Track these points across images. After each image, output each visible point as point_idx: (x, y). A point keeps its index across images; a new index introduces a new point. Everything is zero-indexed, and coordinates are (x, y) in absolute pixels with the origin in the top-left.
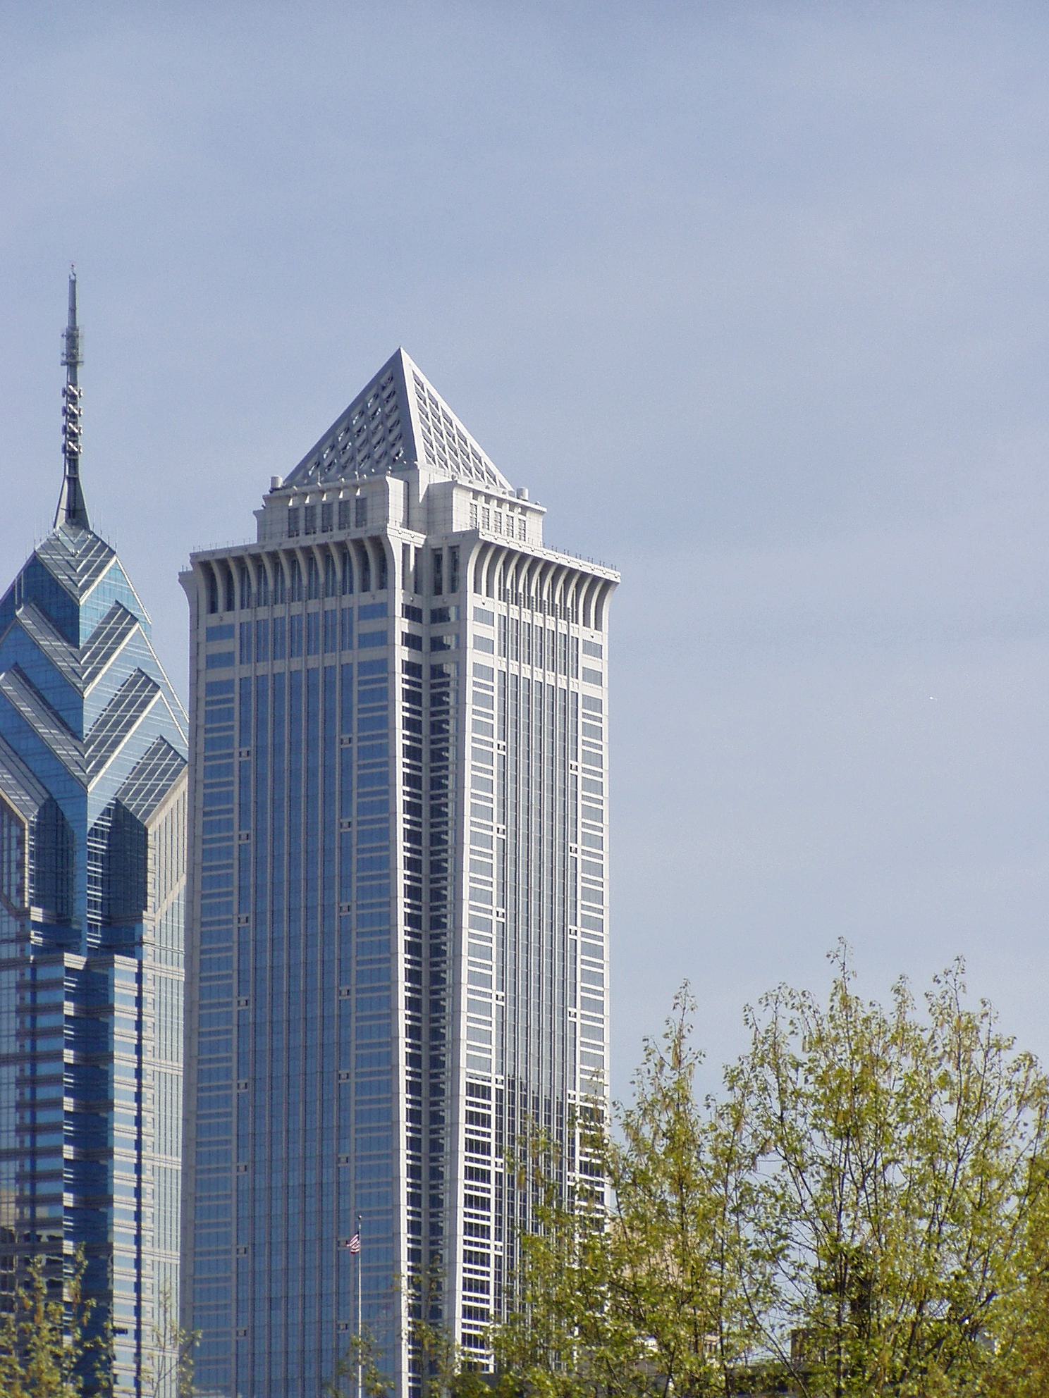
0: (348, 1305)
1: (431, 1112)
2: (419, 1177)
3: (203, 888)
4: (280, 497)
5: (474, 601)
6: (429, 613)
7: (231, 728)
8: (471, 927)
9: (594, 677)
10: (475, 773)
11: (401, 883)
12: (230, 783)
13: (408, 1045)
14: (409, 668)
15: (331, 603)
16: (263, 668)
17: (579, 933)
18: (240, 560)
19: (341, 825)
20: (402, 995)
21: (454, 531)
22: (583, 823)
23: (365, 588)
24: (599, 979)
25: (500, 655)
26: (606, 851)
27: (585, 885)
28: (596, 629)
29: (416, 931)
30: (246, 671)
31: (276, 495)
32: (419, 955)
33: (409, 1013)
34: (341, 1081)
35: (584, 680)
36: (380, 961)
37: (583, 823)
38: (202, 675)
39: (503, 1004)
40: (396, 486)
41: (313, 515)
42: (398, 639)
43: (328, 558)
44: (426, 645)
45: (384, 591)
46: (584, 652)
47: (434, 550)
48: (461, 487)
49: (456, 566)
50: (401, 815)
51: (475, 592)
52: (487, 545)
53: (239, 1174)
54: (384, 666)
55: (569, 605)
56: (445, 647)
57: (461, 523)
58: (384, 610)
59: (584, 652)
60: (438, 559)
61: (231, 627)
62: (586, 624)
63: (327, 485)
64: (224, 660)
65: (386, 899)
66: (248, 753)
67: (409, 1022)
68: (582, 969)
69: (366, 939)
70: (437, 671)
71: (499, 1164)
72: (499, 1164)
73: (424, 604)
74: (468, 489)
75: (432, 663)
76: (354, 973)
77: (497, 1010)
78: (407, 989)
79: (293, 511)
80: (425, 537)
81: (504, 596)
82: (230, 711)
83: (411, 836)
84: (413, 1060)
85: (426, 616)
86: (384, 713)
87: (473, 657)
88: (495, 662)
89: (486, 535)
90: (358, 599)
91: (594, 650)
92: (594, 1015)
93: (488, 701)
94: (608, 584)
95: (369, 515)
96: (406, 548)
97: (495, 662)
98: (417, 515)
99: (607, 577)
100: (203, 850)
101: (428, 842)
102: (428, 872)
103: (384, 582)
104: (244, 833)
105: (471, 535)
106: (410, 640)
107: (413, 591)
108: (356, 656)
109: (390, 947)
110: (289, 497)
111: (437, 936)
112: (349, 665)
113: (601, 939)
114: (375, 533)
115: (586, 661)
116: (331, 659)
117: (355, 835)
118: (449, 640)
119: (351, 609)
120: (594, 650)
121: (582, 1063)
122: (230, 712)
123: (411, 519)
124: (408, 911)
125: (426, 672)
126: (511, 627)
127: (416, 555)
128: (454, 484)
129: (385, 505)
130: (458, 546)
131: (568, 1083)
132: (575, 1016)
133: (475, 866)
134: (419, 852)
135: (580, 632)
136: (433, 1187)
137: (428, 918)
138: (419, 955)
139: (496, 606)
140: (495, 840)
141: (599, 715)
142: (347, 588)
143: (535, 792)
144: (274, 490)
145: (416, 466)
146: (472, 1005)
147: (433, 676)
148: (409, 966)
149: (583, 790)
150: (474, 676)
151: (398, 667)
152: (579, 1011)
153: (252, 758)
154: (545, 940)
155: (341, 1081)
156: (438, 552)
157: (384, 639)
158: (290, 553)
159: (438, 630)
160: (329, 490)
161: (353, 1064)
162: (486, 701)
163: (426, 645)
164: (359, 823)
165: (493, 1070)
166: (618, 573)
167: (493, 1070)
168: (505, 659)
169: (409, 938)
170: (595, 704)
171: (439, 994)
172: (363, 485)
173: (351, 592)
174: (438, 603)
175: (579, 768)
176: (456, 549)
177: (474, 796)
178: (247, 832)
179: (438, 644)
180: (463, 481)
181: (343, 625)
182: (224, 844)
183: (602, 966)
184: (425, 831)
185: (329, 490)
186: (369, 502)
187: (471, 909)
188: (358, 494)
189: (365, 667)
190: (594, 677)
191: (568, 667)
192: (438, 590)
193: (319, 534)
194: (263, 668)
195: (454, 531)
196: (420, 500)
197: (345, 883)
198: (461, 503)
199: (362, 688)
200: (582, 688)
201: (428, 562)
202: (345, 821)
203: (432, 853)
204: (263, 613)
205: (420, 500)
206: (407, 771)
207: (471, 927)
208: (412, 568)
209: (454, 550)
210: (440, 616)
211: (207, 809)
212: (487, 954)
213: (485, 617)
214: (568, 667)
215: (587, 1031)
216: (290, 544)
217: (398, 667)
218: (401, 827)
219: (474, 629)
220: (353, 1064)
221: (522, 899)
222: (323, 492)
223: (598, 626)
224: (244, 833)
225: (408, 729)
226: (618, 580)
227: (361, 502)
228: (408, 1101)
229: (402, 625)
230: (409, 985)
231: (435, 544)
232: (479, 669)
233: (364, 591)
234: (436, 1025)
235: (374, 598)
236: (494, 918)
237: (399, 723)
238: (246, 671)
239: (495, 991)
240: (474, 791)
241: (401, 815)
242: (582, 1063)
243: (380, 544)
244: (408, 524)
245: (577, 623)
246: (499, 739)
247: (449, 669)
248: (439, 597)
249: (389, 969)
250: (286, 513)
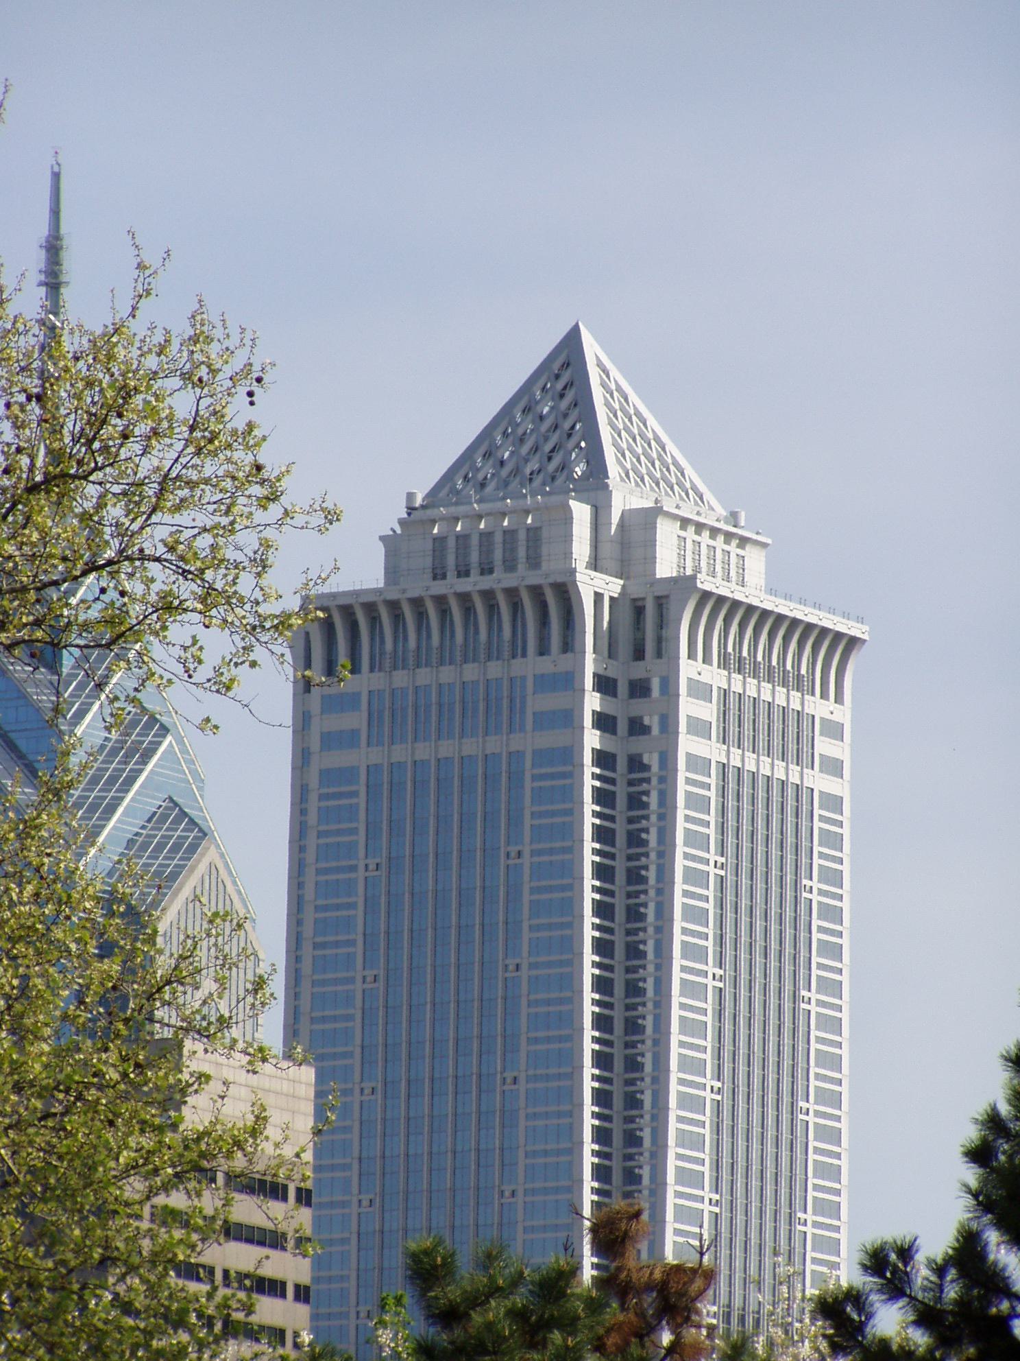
0: (516, 1164)
1: (625, 1131)
2: (610, 1030)
3: (314, 972)
4: (422, 522)
5: (688, 669)
6: (627, 684)
7: (352, 943)
8: (677, 1183)
9: (833, 767)
10: (686, 900)
11: (589, 934)
12: (355, 794)
13: (595, 1154)
14: (602, 758)
15: (495, 669)
16: (400, 753)
17: (811, 1112)
18: (370, 608)
19: (508, 855)
20: (589, 1161)
21: (658, 576)
22: (819, 927)
23: (543, 651)
24: (835, 1173)
25: (718, 742)
26: (845, 1002)
27: (823, 862)
28: (836, 702)
29: (607, 999)
30: (376, 756)
31: (416, 517)
32: (611, 1032)
33: (597, 1072)
34: (506, 1088)
35: (821, 771)
36: (559, 1076)
37: (819, 927)
38: (315, 759)
39: (719, 1098)
40: (581, 512)
41: (467, 547)
42: (588, 720)
43: (492, 608)
44: (622, 727)
45: (569, 655)
46: (821, 734)
47: (634, 600)
48: (669, 515)
49: (665, 621)
50: (589, 881)
51: (689, 658)
52: (706, 595)
53: (363, 1098)
54: (570, 754)
55: (803, 671)
56: (645, 730)
57: (665, 568)
58: (570, 682)
59: (821, 734)
60: (639, 611)
61: (355, 697)
62: (824, 695)
63: (487, 507)
64: (348, 739)
65: (569, 919)
66: (373, 1091)
67: (597, 972)
68: (815, 1198)
69: (541, 1047)
70: (636, 763)
71: (715, 1089)
72: (715, 1089)
73: (621, 673)
74: (675, 517)
75: (632, 678)
76: (523, 1054)
77: (714, 991)
78: (595, 1003)
79: (440, 541)
80: (621, 582)
81: (724, 663)
82: (353, 809)
83: (601, 872)
84: (601, 1097)
85: (622, 689)
86: (568, 932)
87: (687, 744)
88: (712, 750)
89: (706, 583)
90: (531, 666)
91: (834, 730)
92: (828, 1221)
93: (703, 805)
94: (853, 642)
95: (545, 550)
96: (598, 597)
97: (712, 750)
98: (607, 550)
99: (853, 633)
100: (319, 808)
101: (624, 878)
102: (624, 882)
103: (570, 644)
104: (370, 973)
105: (685, 583)
106: (604, 722)
107: (606, 653)
108: (529, 741)
109: (571, 982)
110: (434, 522)
111: (635, 932)
112: (520, 755)
113: (840, 1009)
114: (560, 579)
115: (824, 746)
116: (494, 744)
117: (527, 871)
118: (652, 721)
119: (524, 678)
120: (834, 730)
121: (813, 1250)
122: (352, 810)
123: (600, 555)
124: (597, 897)
125: (622, 764)
126: (732, 701)
127: (610, 607)
128: (657, 511)
129: (568, 538)
130: (667, 597)
131: (798, 1203)
132: (805, 1224)
133: (689, 913)
134: (612, 781)
135: (818, 707)
136: (630, 1082)
137: (624, 832)
138: (611, 1032)
139: (715, 676)
140: (712, 879)
141: (838, 817)
142: (517, 650)
143: (759, 924)
144: (411, 509)
145: (607, 486)
146: (681, 1212)
147: (631, 769)
148: (597, 1009)
149: (819, 918)
150: (687, 770)
151: (588, 758)
152: (810, 1217)
153: (383, 872)
154: (770, 1121)
155: (506, 1088)
156: (640, 603)
157: (570, 719)
158: (440, 600)
159: (637, 707)
160: (488, 514)
161: (527, 838)
162: (701, 804)
163: (622, 727)
164: (532, 966)
165: (709, 1075)
166: (865, 628)
167: (709, 1075)
168: (725, 747)
169: (597, 859)
170: (834, 803)
171: (636, 1009)
172: (537, 509)
173: (524, 655)
174: (638, 671)
175: (812, 999)
176: (664, 601)
177: (683, 1006)
178: (375, 972)
179: (637, 727)
180: (668, 506)
181: (511, 700)
182: (345, 913)
183: (838, 1156)
184: (620, 865)
185: (488, 514)
186: (545, 533)
187: (682, 971)
188: (529, 521)
189: (541, 756)
190: (833, 767)
191: (802, 755)
192: (639, 654)
193: (474, 576)
194: (400, 753)
195: (658, 576)
196: (613, 533)
197: (514, 821)
198: (666, 534)
199: (537, 784)
200: (818, 781)
201: (626, 617)
202: (511, 962)
203: (629, 895)
204: (401, 678)
205: (613, 533)
206: (597, 784)
207: (677, 1183)
208: (605, 625)
209: (661, 602)
210: (639, 689)
211: (319, 939)
212: (698, 1144)
213: (701, 691)
214: (802, 755)
215: (820, 1243)
216: (439, 588)
217: (588, 758)
218: (589, 897)
219: (688, 707)
220: (527, 838)
221: (742, 1068)
222: (480, 517)
223: (839, 699)
224: (370, 973)
225: (598, 803)
226: (865, 637)
227: (534, 534)
228: (595, 889)
229: (593, 702)
230: (597, 996)
231: (636, 591)
232: (696, 763)
233: (541, 654)
234: (632, 1088)
235: (555, 663)
236: (711, 869)
237: (588, 832)
238: (376, 756)
239: (711, 969)
240: (688, 850)
241: (589, 881)
242: (813, 1250)
243: (566, 593)
244: (595, 564)
245: (813, 769)
246: (712, 1079)
247: (652, 759)
248: (641, 663)
249: (571, 1163)
250: (429, 545)
